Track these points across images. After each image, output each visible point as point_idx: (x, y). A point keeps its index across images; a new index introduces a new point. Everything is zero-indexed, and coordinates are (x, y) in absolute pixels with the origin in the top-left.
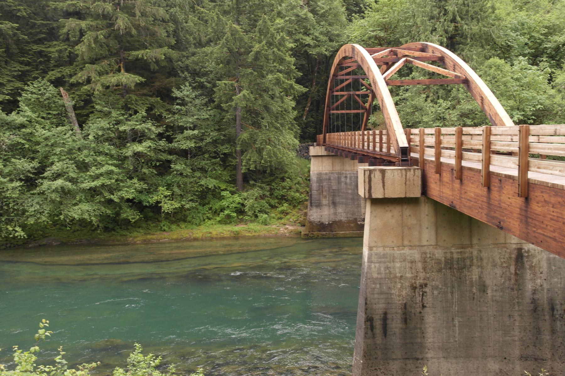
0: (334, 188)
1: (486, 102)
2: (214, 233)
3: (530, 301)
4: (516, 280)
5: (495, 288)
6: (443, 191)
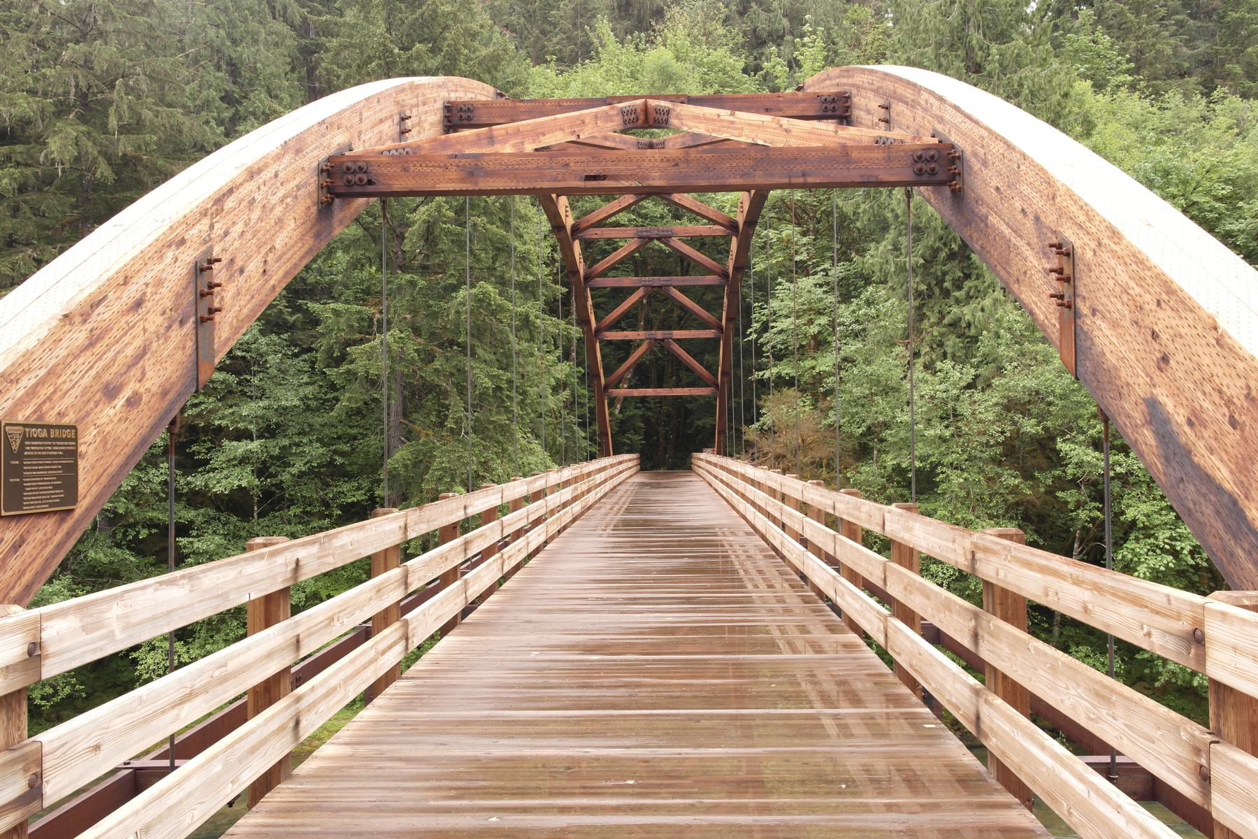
1: (1102, 282)
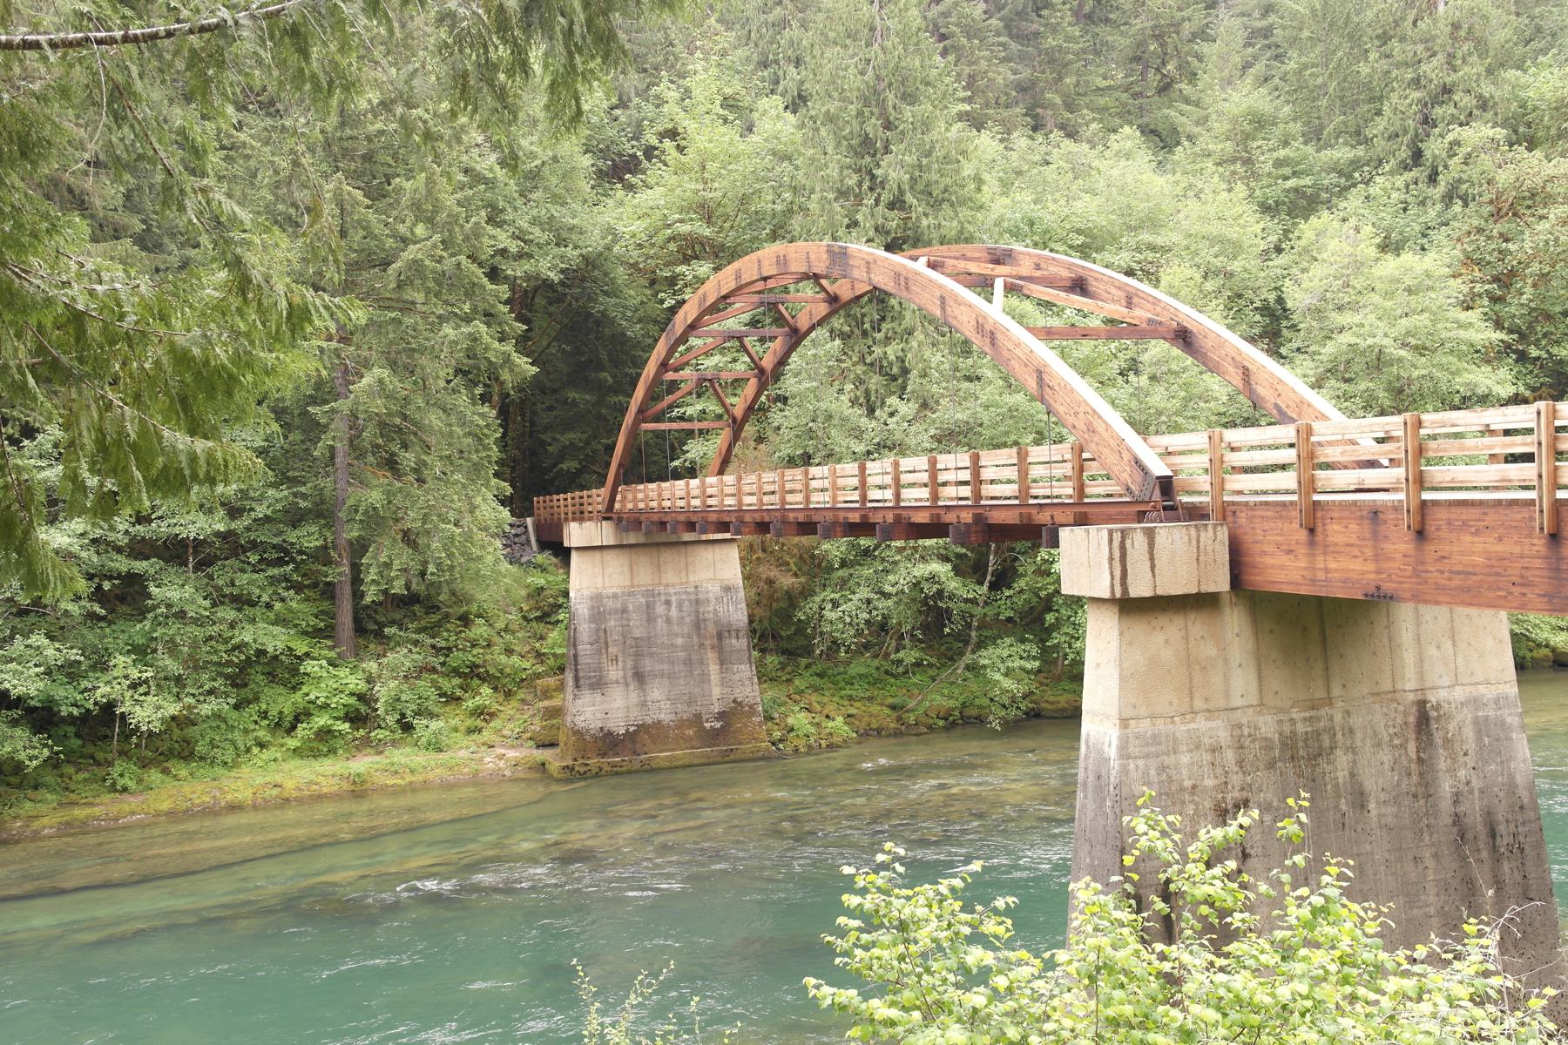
0: (637, 633)
2: (290, 784)
3: (1450, 821)
4: (1421, 775)
5: (1383, 796)
6: (1285, 568)
